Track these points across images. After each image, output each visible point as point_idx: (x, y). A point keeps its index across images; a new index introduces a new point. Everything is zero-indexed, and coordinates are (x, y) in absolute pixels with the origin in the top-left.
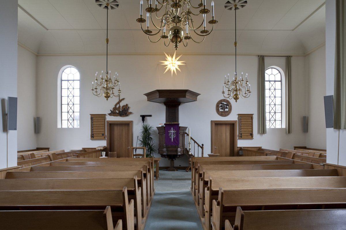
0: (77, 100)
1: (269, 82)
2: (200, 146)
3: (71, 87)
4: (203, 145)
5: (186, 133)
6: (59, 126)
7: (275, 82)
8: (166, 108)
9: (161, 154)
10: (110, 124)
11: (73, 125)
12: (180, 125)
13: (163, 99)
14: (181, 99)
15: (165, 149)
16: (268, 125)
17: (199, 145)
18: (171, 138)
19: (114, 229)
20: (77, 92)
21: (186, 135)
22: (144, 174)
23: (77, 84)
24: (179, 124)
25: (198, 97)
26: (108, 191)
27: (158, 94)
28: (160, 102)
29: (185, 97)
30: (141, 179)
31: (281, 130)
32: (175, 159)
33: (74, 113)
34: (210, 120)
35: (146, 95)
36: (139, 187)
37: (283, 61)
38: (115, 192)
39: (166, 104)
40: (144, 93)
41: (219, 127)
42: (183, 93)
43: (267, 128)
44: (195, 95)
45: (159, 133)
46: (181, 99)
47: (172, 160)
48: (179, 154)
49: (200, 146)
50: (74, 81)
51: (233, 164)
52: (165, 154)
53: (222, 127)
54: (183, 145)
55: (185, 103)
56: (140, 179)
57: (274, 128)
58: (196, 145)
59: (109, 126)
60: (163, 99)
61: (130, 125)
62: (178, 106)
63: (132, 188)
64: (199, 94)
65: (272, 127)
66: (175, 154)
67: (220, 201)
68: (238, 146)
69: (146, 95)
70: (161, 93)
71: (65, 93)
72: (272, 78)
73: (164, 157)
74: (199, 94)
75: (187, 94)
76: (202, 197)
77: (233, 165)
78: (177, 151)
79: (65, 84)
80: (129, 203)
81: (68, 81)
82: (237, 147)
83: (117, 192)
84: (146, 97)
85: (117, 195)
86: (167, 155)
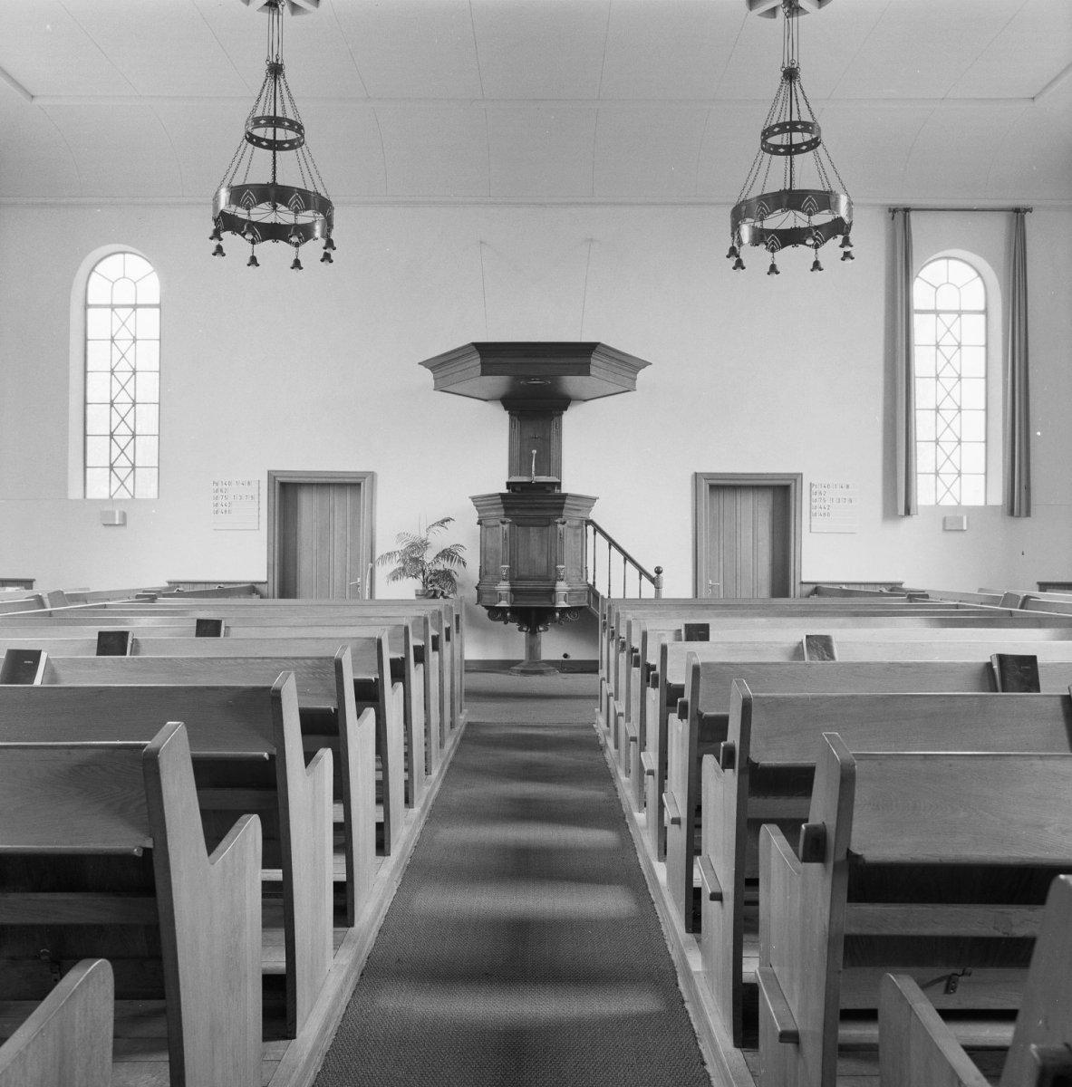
0: (148, 387)
1: (934, 316)
2: (648, 576)
3: (123, 334)
4: (658, 571)
5: (591, 522)
6: (75, 493)
7: (960, 316)
8: (512, 420)
9: (487, 607)
10: (284, 485)
11: (131, 490)
12: (565, 489)
13: (498, 383)
14: (572, 384)
15: (504, 586)
16: (925, 494)
17: (642, 572)
18: (607, 903)
19: (306, 765)
20: (148, 356)
21: (590, 528)
22: (416, 648)
23: (149, 322)
24: (559, 485)
25: (642, 375)
26: (285, 658)
27: (479, 361)
28: (485, 398)
29: (585, 371)
30: (403, 655)
31: (987, 509)
32: (546, 630)
33: (137, 438)
34: (692, 472)
35: (425, 364)
36: (396, 684)
37: (998, 228)
38: (309, 662)
39: (508, 402)
40: (421, 360)
41: (727, 500)
42: (579, 355)
43: (919, 503)
44: (628, 367)
45: (480, 523)
46: (572, 384)
47: (533, 633)
48: (562, 604)
49: (648, 576)
50: (138, 310)
51: (760, 615)
52: (504, 604)
53: (738, 497)
54: (583, 570)
55: (585, 401)
56: (399, 655)
57: (956, 504)
58: (632, 571)
59: (277, 490)
60: (498, 383)
61: (365, 488)
62: (561, 415)
63: (370, 673)
64: (645, 364)
65: (949, 501)
66: (546, 604)
67: (689, 699)
68: (804, 579)
69: (425, 364)
70: (491, 355)
71: (99, 357)
72: (947, 300)
73: (500, 619)
74: (645, 364)
75: (596, 362)
76: (638, 735)
77: (763, 620)
78: (551, 592)
79: (99, 323)
80: (358, 716)
81: (113, 307)
82: (802, 583)
83: (316, 662)
84: (428, 376)
85: (313, 674)
86: (511, 609)
